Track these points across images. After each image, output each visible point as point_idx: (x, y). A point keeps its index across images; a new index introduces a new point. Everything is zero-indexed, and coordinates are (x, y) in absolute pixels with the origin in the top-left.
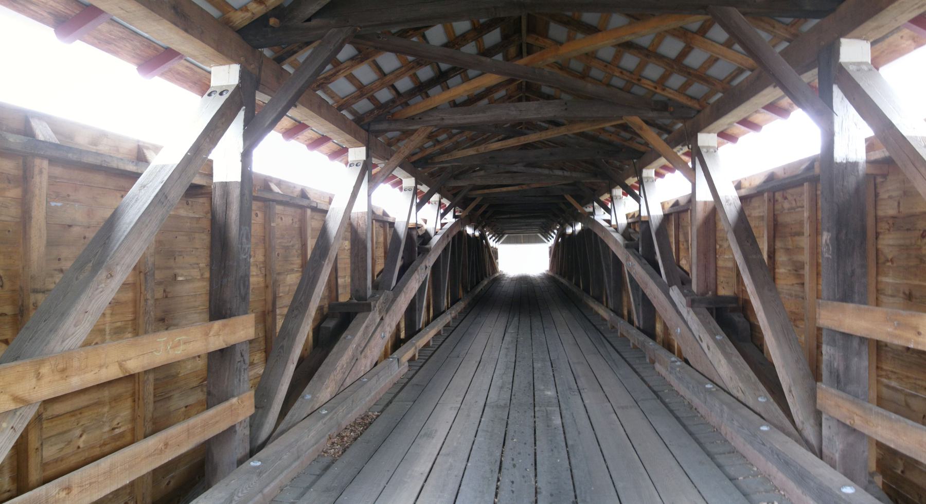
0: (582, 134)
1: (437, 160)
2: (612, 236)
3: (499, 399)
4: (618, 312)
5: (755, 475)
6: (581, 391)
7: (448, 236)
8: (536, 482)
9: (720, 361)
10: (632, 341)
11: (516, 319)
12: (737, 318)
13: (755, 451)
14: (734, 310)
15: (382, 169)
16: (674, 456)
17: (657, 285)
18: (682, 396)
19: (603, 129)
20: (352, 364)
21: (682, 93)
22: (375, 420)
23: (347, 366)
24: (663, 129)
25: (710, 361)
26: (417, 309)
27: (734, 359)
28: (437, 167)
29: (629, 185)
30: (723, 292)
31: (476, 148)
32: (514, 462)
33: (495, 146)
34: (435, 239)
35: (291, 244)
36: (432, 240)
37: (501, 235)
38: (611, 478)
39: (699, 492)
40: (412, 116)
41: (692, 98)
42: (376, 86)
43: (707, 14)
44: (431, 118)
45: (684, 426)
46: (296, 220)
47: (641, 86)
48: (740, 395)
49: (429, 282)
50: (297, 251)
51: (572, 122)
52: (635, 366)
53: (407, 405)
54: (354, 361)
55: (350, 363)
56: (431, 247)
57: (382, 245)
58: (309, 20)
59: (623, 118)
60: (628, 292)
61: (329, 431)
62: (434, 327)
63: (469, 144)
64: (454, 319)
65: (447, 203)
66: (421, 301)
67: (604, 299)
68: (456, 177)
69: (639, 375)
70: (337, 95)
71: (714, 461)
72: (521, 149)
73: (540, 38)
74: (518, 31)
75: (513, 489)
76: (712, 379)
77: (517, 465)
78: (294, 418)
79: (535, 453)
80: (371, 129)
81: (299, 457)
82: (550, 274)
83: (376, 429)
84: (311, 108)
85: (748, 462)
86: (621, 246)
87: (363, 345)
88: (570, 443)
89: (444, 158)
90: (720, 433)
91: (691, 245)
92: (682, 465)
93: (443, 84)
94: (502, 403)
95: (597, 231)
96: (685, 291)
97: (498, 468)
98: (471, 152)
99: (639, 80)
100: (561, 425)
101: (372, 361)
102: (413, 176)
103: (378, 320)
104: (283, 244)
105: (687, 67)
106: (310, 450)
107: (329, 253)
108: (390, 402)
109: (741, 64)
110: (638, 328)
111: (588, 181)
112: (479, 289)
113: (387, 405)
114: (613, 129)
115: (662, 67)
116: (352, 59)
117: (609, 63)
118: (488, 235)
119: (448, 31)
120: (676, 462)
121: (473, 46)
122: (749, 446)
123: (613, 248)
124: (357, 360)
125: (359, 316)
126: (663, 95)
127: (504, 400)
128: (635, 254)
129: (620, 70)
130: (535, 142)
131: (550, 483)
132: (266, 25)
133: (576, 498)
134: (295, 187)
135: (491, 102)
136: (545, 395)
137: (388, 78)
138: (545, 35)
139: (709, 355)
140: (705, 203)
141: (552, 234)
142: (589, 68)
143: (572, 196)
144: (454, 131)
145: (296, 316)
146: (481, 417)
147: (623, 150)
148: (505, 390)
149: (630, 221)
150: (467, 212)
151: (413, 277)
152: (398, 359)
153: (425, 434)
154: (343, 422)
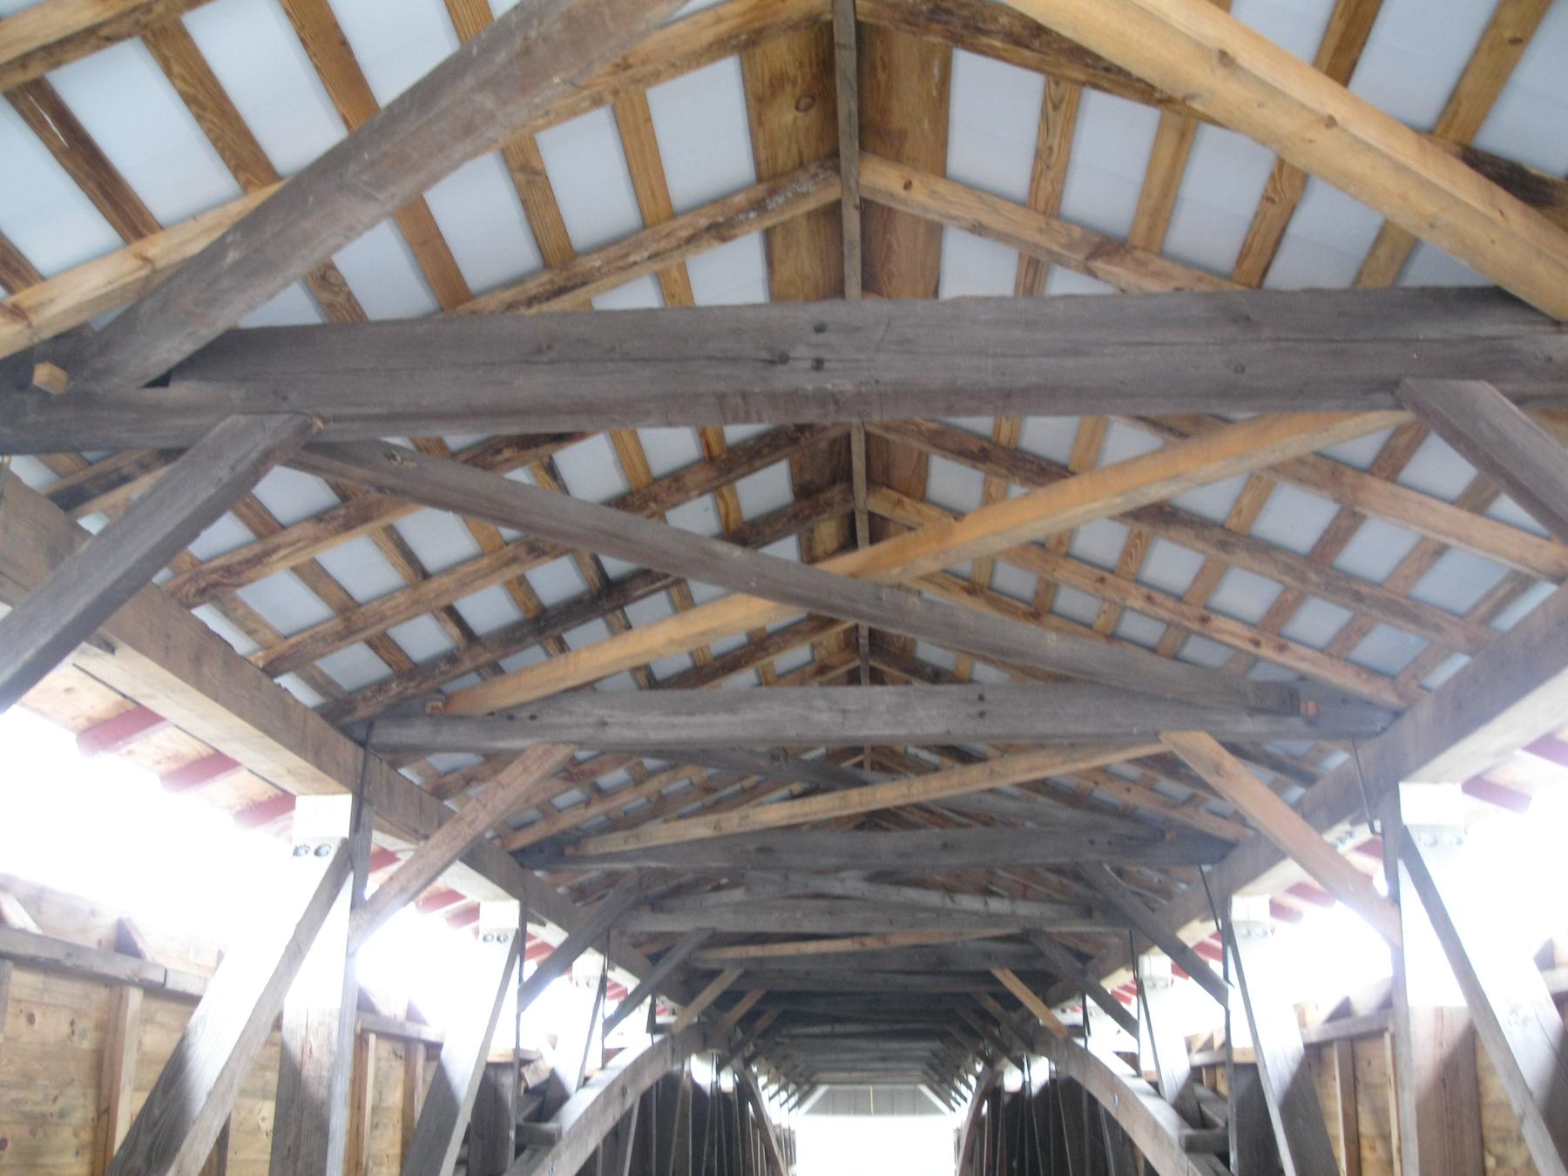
0: (1041, 787)
1: (593, 847)
2: (1142, 1106)
7: (623, 1093)
15: (410, 863)
19: (1103, 770)
21: (1338, 658)
24: (1288, 770)
28: (594, 872)
29: (1190, 944)
31: (712, 818)
33: (773, 813)
35: (56, 1108)
37: (806, 1088)
40: (508, 709)
41: (1373, 672)
42: (397, 606)
43: (1399, 406)
44: (566, 719)
46: (85, 1024)
47: (1211, 639)
50: (76, 1134)
51: (1009, 748)
56: (560, 1131)
57: (396, 1117)
58: (163, 381)
59: (1161, 737)
63: (697, 804)
65: (626, 980)
68: (657, 904)
70: (267, 626)
72: (860, 827)
73: (906, 500)
74: (843, 475)
80: (374, 740)
84: (165, 658)
86: (1171, 1145)
89: (616, 842)
91: (1399, 1150)
93: (610, 616)
95: (1094, 1088)
98: (699, 829)
99: (1204, 620)
102: (514, 895)
104: (27, 1108)
105: (1349, 577)
107: (184, 1147)
109: (1521, 561)
111: (1064, 929)
114: (1133, 772)
115: (1272, 578)
116: (319, 517)
117: (1112, 572)
119: (629, 456)
121: (706, 510)
123: (1147, 1147)
126: (1284, 666)
129: (1145, 590)
130: (901, 808)
132: (24, 385)
134: (93, 913)
135: (767, 680)
137: (434, 585)
138: (916, 490)
140: (1440, 1014)
141: (963, 1089)
142: (1048, 588)
143: (1020, 975)
144: (650, 763)
147: (1168, 837)
149: (1199, 1059)
150: (692, 1015)
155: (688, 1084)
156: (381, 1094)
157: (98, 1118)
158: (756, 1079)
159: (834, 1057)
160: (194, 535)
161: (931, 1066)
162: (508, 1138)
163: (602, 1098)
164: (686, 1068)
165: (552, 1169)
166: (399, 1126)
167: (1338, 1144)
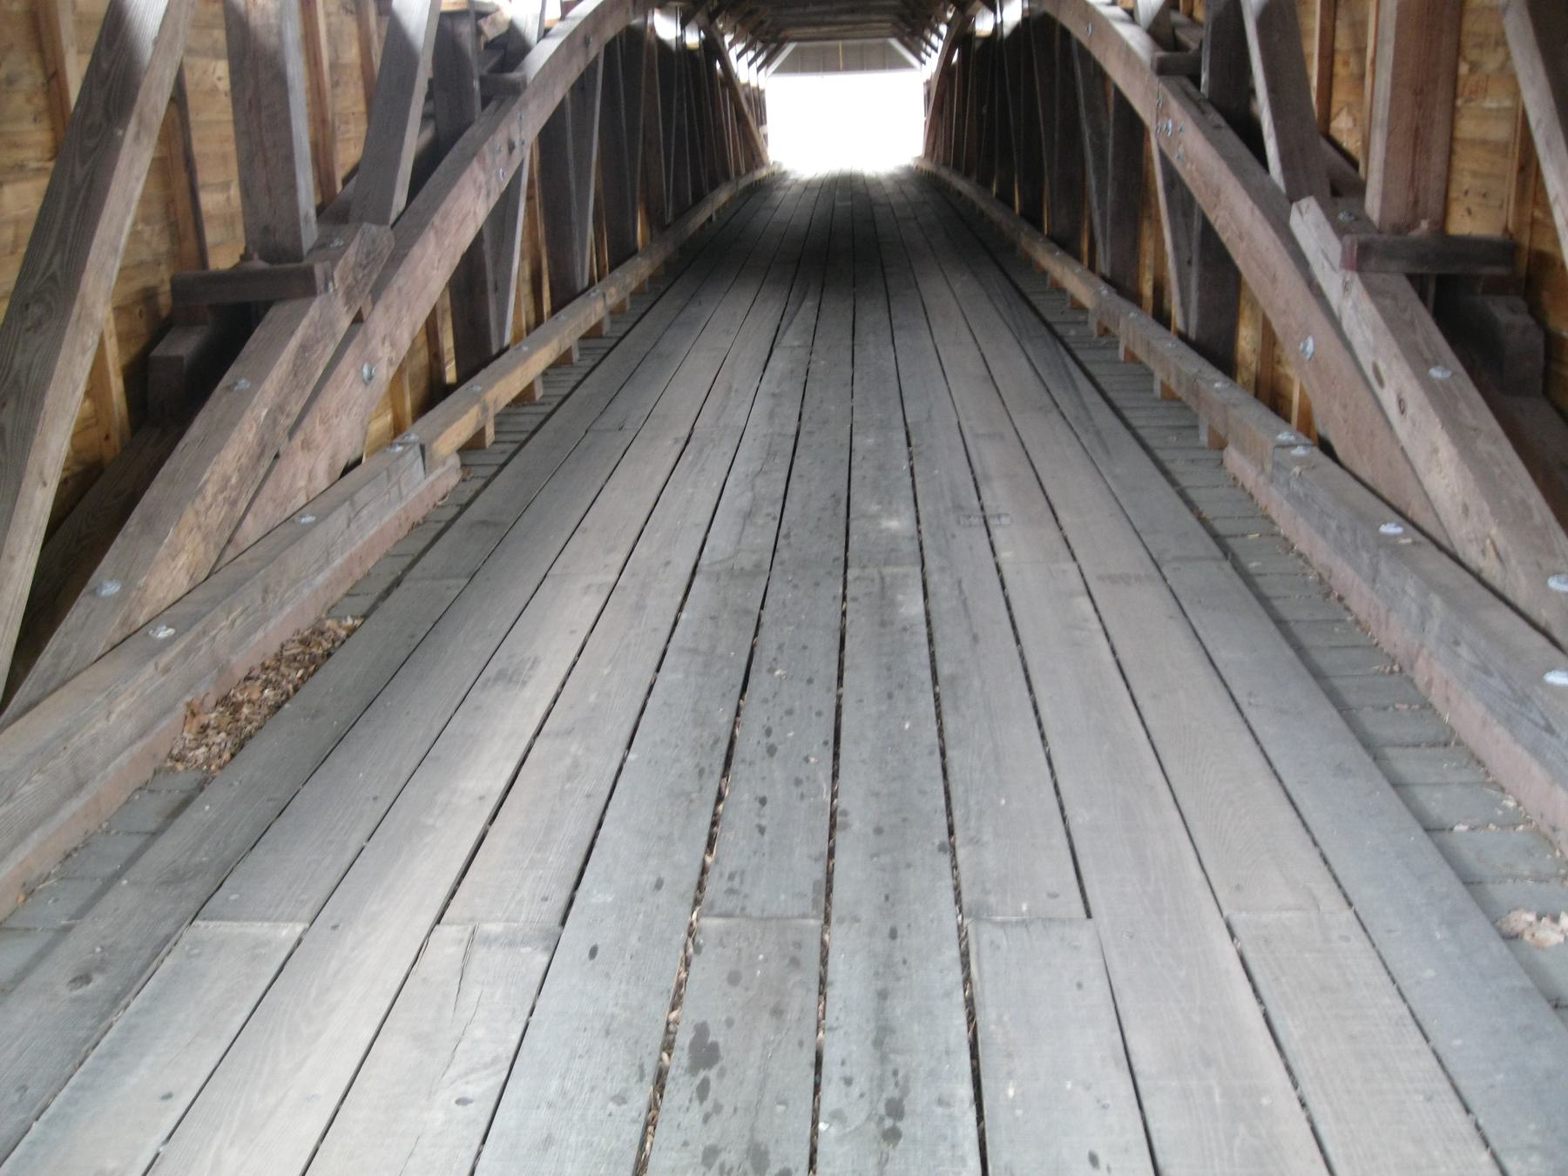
3: (737, 552)
4: (1123, 285)
5: (1509, 823)
6: (992, 522)
7: (586, 42)
8: (834, 795)
9: (1435, 451)
10: (1159, 376)
11: (810, 304)
12: (1506, 314)
13: (1519, 749)
14: (1497, 287)
16: (1257, 742)
17: (1250, 197)
18: (1300, 555)
20: (262, 472)
22: (343, 642)
23: (242, 480)
25: (1402, 449)
26: (490, 286)
27: (1483, 446)
30: (1468, 223)
32: (772, 740)
34: (542, 54)
36: (532, 52)
37: (773, 46)
38: (1058, 793)
39: (1326, 861)
45: (1299, 650)
48: (1489, 566)
49: (530, 198)
50: (29, 100)
52: (1161, 455)
53: (448, 588)
54: (266, 462)
55: (254, 468)
60: (1159, 221)
61: (187, 691)
62: (545, 342)
64: (616, 312)
66: (503, 257)
67: (1085, 247)
69: (1173, 483)
71: (1380, 768)
75: (764, 822)
76: (1403, 508)
77: (780, 747)
78: (66, 662)
79: (839, 708)
81: (80, 786)
82: (927, 166)
83: (342, 672)
85: (1490, 779)
86: (1142, 69)
87: (295, 408)
88: (944, 670)
90: (1412, 680)
91: (1374, 62)
92: (1280, 771)
94: (747, 561)
96: (1341, 216)
97: (723, 760)
100: (923, 619)
101: (333, 457)
103: (345, 322)
106: (124, 758)
108: (397, 582)
110: (1183, 337)
112: (701, 217)
113: (387, 592)
118: (731, 44)
120: (1263, 761)
122: (1500, 731)
123: (1117, 73)
124: (277, 456)
125: (276, 314)
127: (754, 552)
128: (1188, 95)
131: (877, 795)
133: (951, 832)
136: (881, 531)
139: (1402, 428)
145: (38, 324)
146: (681, 609)
148: (760, 521)
151: (466, 179)
152: (422, 448)
153: (501, 675)
154: (234, 659)
155: (653, 39)
156: (336, 51)
157: (49, 81)
158: (723, 36)
159: (801, 10)
160: (152, 349)
161: (902, 17)
162: (473, 90)
163: (565, 46)
164: (649, 22)
165: (521, 118)
166: (360, 83)
167: (1312, 62)
